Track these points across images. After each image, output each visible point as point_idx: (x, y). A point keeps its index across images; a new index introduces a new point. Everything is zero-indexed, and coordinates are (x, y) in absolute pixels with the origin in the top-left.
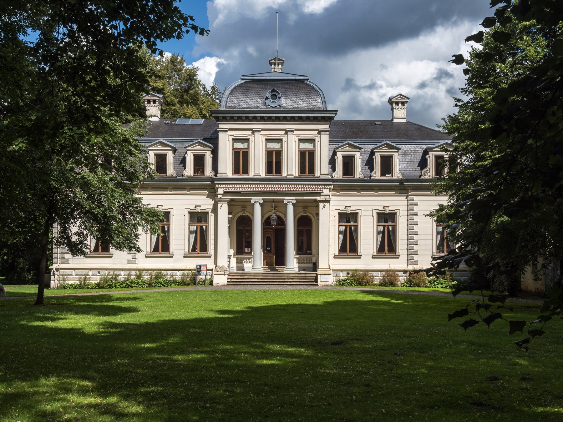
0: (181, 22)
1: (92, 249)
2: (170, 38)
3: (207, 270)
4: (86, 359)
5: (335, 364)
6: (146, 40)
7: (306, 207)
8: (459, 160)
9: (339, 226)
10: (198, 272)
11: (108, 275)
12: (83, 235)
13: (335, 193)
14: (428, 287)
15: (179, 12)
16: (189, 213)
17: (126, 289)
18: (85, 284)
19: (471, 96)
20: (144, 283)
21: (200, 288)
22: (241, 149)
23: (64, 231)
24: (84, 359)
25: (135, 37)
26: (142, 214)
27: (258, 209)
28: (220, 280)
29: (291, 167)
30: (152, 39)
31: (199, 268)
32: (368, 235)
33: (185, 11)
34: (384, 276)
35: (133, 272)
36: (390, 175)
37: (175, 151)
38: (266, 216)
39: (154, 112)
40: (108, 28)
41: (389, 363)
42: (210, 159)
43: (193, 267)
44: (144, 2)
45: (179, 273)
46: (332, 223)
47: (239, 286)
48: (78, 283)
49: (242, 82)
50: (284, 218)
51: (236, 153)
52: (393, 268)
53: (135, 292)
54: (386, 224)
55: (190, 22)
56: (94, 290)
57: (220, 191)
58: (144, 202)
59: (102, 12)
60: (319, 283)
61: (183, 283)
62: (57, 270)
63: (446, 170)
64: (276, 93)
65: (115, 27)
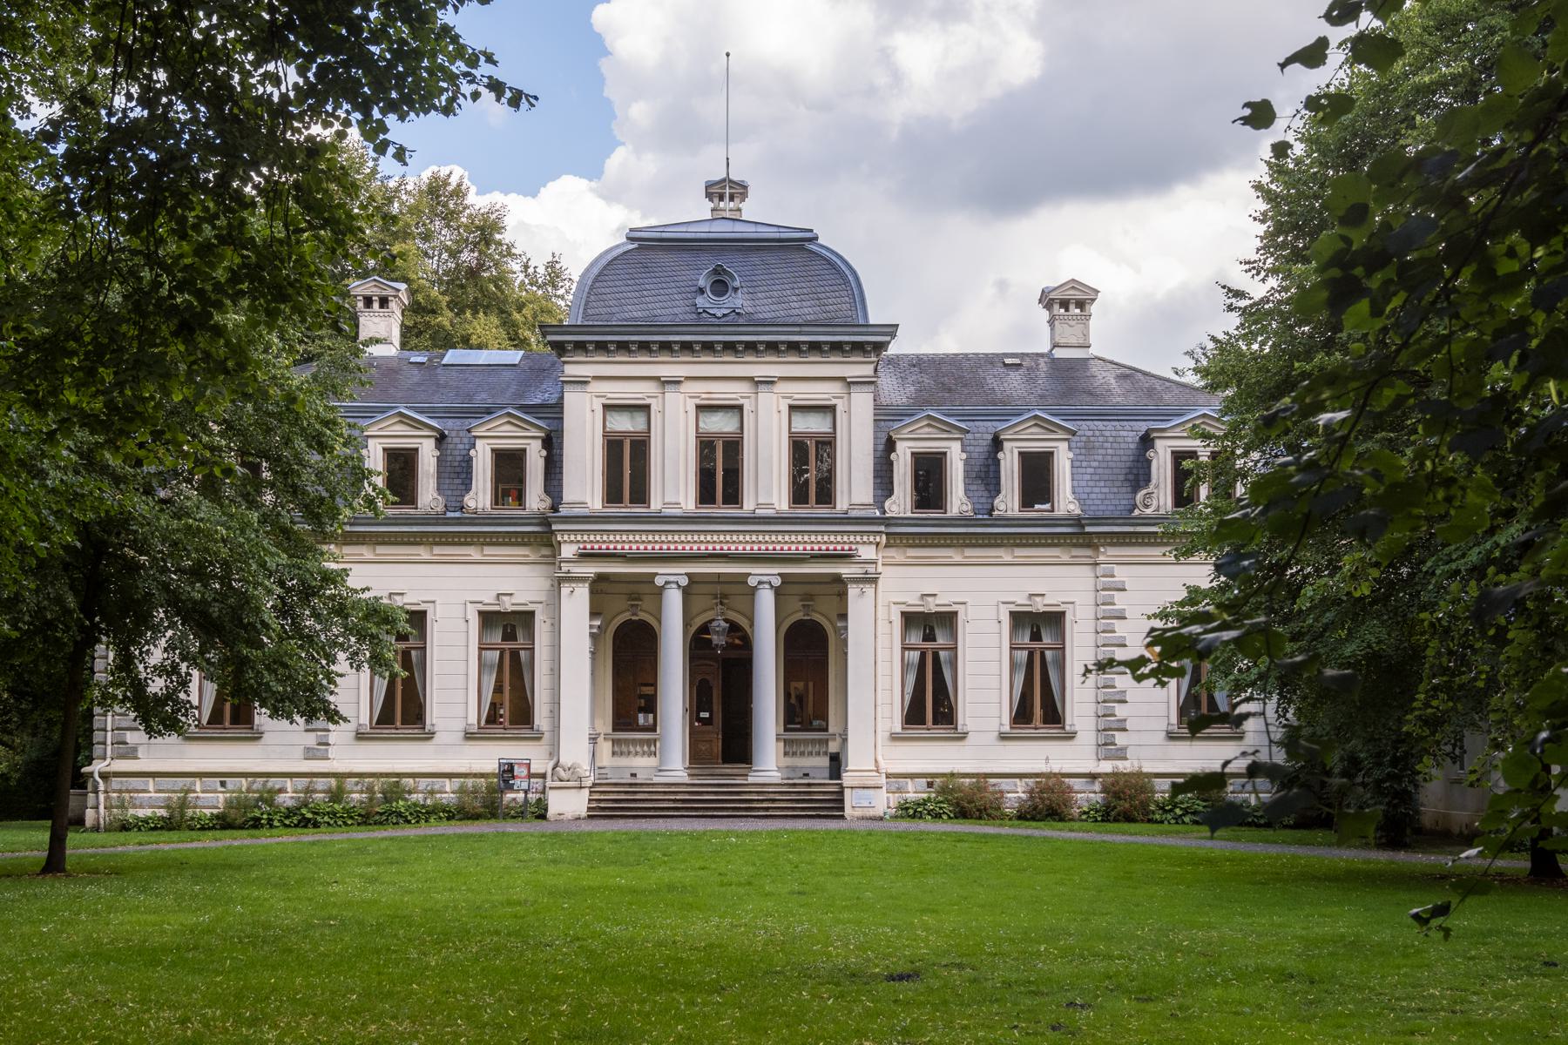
0: (460, 67)
1: (205, 721)
2: (426, 112)
3: (530, 776)
4: (189, 1020)
5: (900, 1033)
6: (358, 116)
7: (809, 597)
8: (1239, 463)
9: (904, 649)
10: (506, 782)
11: (249, 790)
12: (179, 674)
13: (896, 555)
14: (1156, 822)
15: (455, 39)
16: (481, 613)
17: (299, 830)
18: (182, 815)
19: (1273, 282)
20: (349, 812)
21: (511, 827)
22: (625, 434)
23: (126, 663)
24: (184, 1022)
25: (329, 108)
26: (346, 617)
27: (674, 603)
28: (568, 804)
29: (768, 483)
30: (376, 114)
31: (508, 771)
32: (985, 677)
33: (472, 39)
34: (1031, 792)
35: (321, 783)
36: (1047, 506)
37: (441, 439)
38: (698, 622)
39: (382, 330)
40: (253, 81)
41: (1054, 1028)
42: (541, 463)
43: (491, 766)
44: (358, 11)
45: (448, 785)
46: (883, 640)
47: (621, 822)
48: (163, 812)
49: (631, 247)
51: (613, 446)
52: (1056, 767)
53: (326, 838)
54: (1036, 645)
55: (484, 69)
56: (210, 833)
57: (568, 551)
58: (351, 582)
59: (238, 39)
60: (848, 811)
61: (458, 814)
62: (105, 776)
63: (1204, 491)
64: (726, 278)
65: (276, 80)
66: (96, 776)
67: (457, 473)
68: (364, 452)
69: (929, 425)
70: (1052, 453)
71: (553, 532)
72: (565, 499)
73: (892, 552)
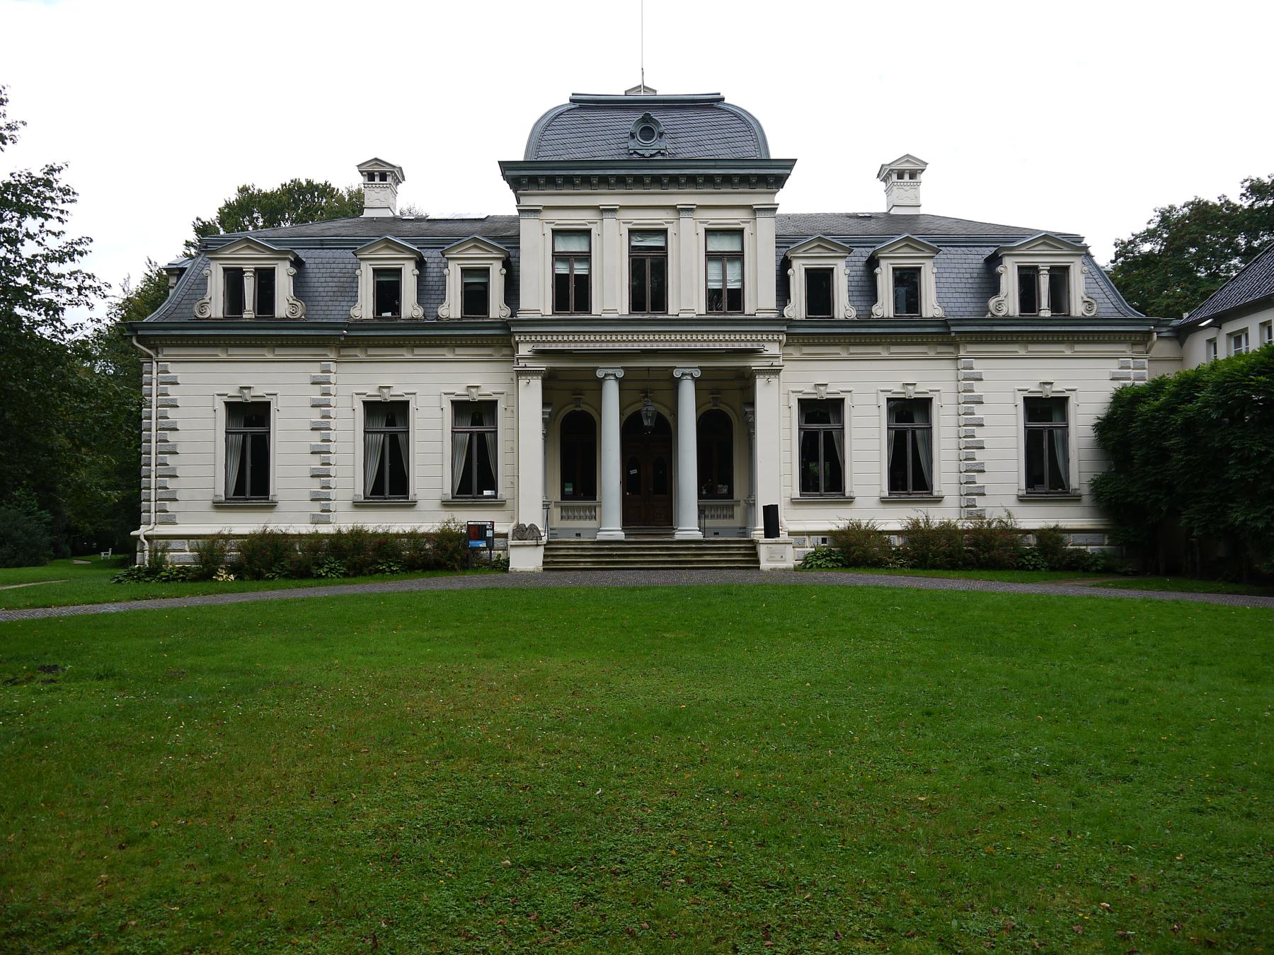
13: (795, 352)
28: (526, 560)
38: (629, 412)
50: (670, 419)
57: (524, 350)
66: (142, 538)
67: (429, 291)
68: (446, 271)
69: (475, 247)
70: (919, 269)
71: (512, 334)
72: (521, 307)
73: (790, 350)
